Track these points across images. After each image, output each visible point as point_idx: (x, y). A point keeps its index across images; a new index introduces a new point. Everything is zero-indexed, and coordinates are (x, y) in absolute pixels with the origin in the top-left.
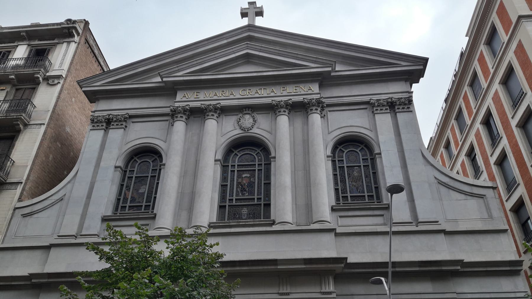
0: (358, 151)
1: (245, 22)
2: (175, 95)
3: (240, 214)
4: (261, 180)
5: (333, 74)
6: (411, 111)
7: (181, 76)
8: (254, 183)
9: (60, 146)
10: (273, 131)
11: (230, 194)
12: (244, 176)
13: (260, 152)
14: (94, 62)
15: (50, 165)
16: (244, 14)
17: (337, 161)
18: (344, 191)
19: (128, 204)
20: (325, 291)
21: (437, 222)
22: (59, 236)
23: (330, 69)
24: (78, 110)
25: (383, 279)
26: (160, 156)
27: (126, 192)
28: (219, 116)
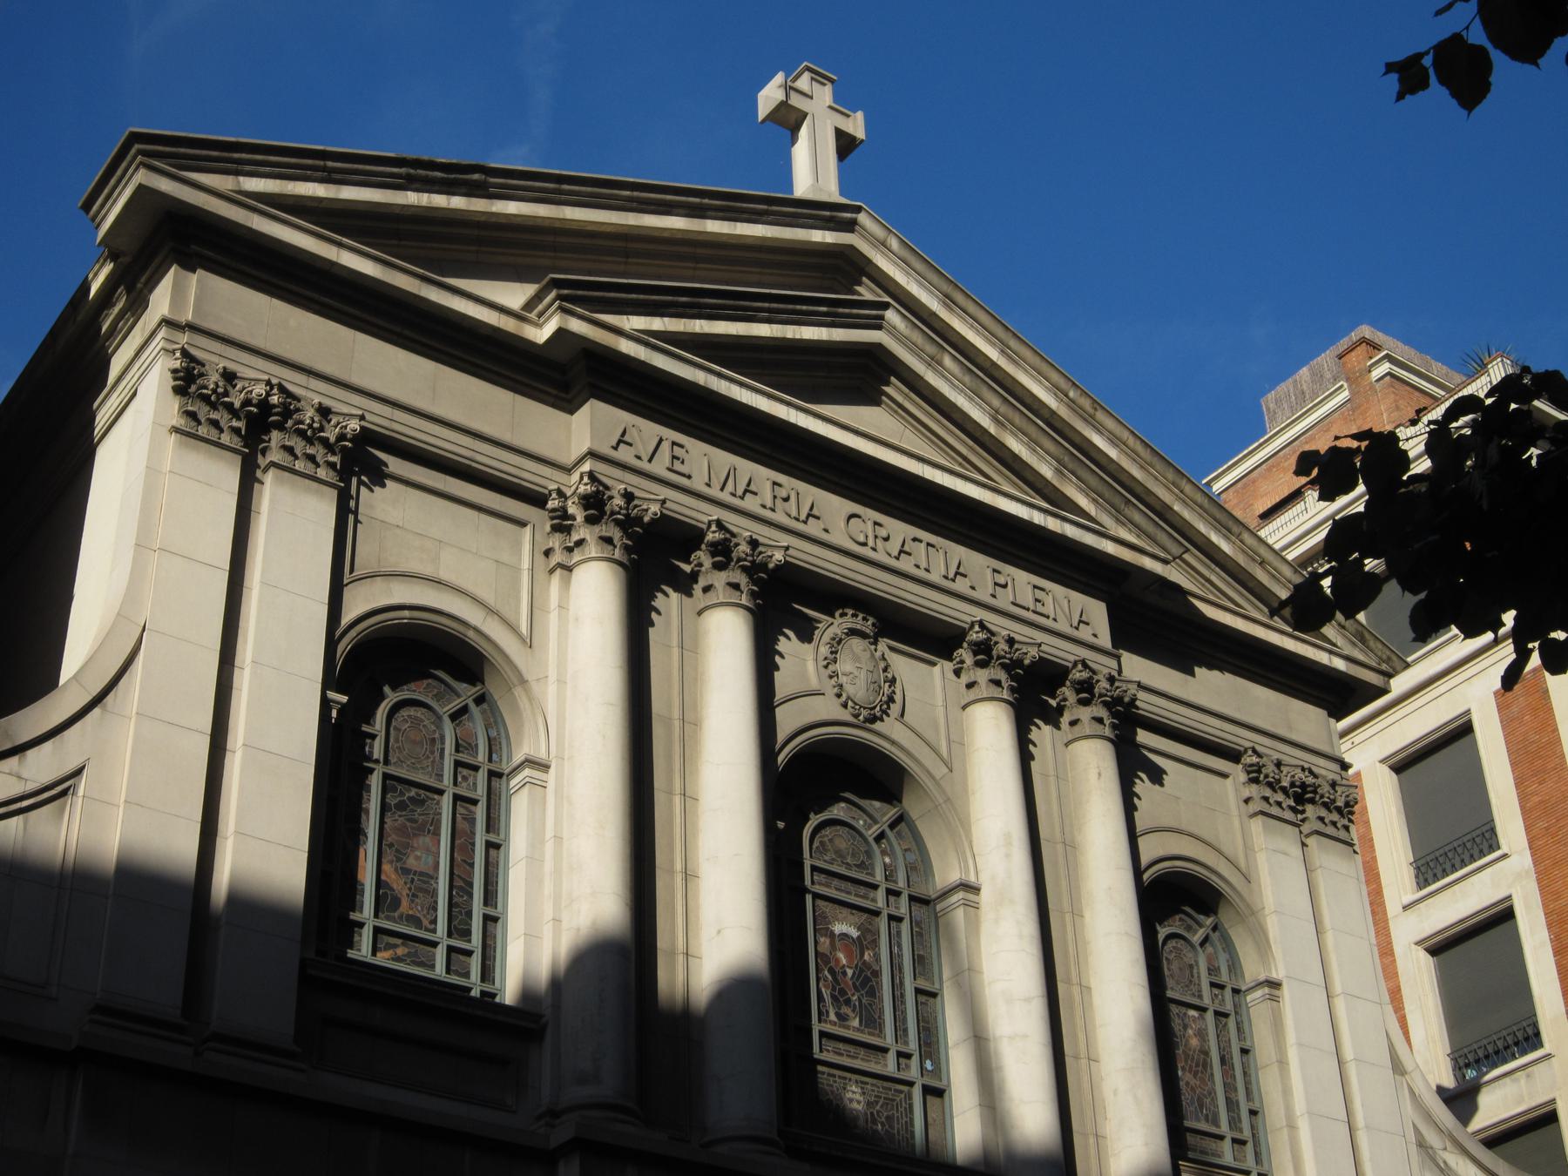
7: (631, 334)
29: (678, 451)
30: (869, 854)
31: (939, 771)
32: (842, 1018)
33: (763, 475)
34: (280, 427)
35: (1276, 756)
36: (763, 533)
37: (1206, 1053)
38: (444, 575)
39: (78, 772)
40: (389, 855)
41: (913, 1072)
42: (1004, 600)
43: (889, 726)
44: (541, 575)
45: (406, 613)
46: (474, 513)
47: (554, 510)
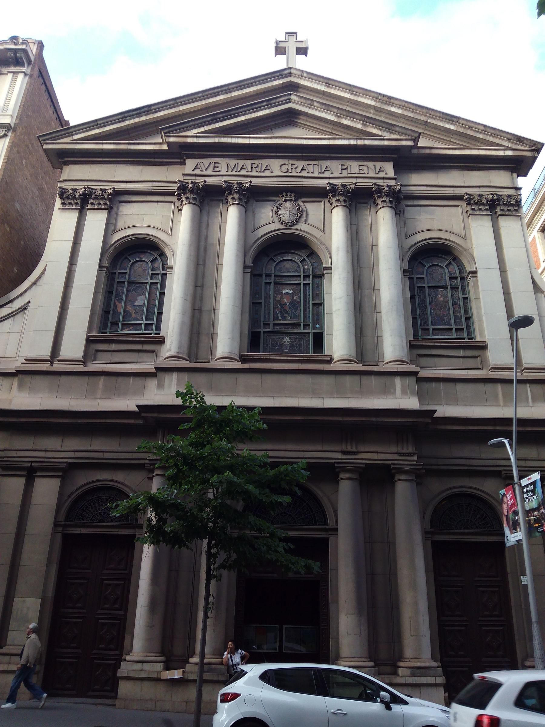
0: (444, 265)
1: (279, 63)
2: (183, 164)
4: (309, 299)
5: (415, 151)
6: (519, 216)
7: (192, 136)
8: (299, 302)
9: (8, 229)
10: (325, 229)
11: (265, 316)
12: (284, 292)
13: (306, 259)
14: (48, 106)
16: (280, 50)
17: (415, 278)
18: (424, 321)
19: (121, 321)
20: (408, 452)
22: (26, 360)
23: (411, 143)
24: (29, 178)
25: (505, 441)
26: (162, 255)
27: (117, 303)
28: (248, 201)
29: (216, 165)
30: (299, 267)
32: (284, 318)
33: (248, 163)
34: (499, 204)
37: (447, 302)
38: (145, 223)
39: (29, 302)
40: (129, 303)
41: (311, 330)
42: (345, 173)
43: (302, 226)
44: (466, 219)
45: (131, 237)
46: (155, 204)
47: (466, 199)
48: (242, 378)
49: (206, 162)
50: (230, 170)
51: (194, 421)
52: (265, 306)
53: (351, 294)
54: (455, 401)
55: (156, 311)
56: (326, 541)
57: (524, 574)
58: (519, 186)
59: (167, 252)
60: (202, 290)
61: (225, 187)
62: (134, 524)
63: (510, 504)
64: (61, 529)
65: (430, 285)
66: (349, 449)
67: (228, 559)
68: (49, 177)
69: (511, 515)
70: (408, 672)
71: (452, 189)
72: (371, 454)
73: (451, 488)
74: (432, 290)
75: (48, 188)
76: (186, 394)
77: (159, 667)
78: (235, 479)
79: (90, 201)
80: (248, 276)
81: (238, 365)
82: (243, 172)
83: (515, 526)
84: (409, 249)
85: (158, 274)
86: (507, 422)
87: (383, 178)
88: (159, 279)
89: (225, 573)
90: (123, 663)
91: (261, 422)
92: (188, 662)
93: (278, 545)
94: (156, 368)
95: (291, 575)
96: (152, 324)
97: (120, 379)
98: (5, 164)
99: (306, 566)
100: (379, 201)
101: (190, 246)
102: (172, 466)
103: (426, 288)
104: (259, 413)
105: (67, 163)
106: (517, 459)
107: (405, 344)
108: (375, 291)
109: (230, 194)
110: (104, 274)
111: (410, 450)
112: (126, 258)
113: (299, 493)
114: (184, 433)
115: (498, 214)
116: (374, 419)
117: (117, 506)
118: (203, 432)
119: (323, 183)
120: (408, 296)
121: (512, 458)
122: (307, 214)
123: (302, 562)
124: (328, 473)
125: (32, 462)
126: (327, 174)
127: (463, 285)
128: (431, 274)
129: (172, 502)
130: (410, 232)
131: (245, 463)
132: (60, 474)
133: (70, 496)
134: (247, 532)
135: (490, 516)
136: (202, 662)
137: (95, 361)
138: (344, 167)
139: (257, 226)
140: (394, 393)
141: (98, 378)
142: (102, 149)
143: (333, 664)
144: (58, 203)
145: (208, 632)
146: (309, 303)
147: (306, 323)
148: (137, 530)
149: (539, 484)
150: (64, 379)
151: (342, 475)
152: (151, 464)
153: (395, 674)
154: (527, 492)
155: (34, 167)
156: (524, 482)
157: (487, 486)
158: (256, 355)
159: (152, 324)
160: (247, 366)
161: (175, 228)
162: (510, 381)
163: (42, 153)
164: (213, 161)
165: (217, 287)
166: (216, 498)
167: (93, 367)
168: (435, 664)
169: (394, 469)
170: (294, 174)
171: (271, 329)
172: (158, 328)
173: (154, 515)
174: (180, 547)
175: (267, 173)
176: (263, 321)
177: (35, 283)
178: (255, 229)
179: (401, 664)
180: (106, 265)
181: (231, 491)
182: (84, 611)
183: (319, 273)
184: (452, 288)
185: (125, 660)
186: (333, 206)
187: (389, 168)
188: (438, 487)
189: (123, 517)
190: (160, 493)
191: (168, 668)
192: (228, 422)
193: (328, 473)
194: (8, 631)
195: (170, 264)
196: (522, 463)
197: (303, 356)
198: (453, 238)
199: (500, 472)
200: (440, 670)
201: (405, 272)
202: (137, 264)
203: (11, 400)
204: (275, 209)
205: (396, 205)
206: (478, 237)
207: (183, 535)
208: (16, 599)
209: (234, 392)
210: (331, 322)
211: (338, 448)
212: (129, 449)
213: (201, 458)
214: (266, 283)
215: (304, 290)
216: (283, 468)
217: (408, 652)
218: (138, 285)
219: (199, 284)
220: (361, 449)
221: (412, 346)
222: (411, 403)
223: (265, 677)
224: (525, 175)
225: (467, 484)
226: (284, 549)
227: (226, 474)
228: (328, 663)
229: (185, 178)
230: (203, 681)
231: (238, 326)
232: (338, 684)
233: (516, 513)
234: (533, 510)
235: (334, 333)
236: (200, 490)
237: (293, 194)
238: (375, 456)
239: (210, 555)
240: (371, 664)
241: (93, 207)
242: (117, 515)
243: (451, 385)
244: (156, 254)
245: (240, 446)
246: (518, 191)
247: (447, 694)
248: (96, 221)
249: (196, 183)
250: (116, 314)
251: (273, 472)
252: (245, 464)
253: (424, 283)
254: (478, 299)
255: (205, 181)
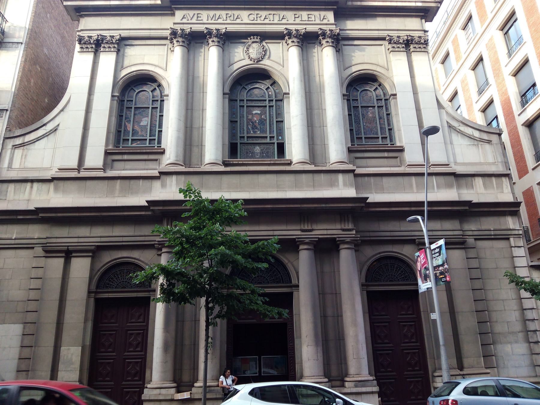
2: (173, 15)
3: (253, 153)
8: (266, 120)
9: (39, 69)
12: (254, 112)
13: (270, 87)
15: (32, 91)
18: (359, 132)
19: (130, 138)
20: (348, 228)
21: (448, 165)
22: (59, 169)
24: (54, 28)
25: (419, 217)
27: (127, 123)
28: (225, 43)
29: (199, 15)
30: (265, 93)
31: (279, 68)
32: (255, 132)
34: (412, 43)
35: (397, 35)
36: (218, 27)
37: (375, 117)
38: (145, 62)
39: (59, 125)
40: (136, 124)
41: (275, 141)
42: (298, 21)
46: (153, 46)
48: (225, 178)
49: (191, 13)
50: (210, 19)
51: (193, 211)
52: (240, 124)
53: (305, 113)
54: (382, 190)
55: (157, 129)
56: (291, 294)
57: (434, 311)
58: (426, 29)
59: (164, 83)
60: (192, 113)
61: (207, 33)
62: (149, 289)
63: (422, 263)
64: (93, 295)
65: (362, 105)
66: (306, 228)
67: (221, 311)
68: (69, 27)
69: (423, 271)
70: (352, 384)
71: (377, 32)
72: (323, 230)
73: (380, 253)
74: (364, 109)
75: (69, 36)
76: (187, 191)
77: (173, 391)
78: (227, 251)
79: (103, 45)
80: (227, 100)
81: (222, 168)
82: (220, 21)
83: (426, 278)
84: (347, 78)
85: (158, 101)
86: (421, 204)
87: (326, 24)
88: (158, 105)
89: (218, 320)
90: (145, 390)
91: (243, 211)
92: (193, 386)
93: (258, 299)
94: (161, 173)
95: (267, 320)
96: (155, 139)
97: (133, 182)
98: (33, 17)
99: (278, 313)
100: (324, 42)
101: (181, 78)
102: (178, 244)
103: (360, 107)
104: (242, 204)
105: (82, 16)
106: (428, 231)
107: (345, 150)
108: (322, 110)
109: (210, 38)
110: (115, 102)
111: (350, 226)
112: (132, 89)
113: (272, 260)
114: (185, 220)
115: (411, 51)
116: (324, 205)
117: (137, 276)
118: (200, 219)
119: (281, 28)
120: (347, 113)
121: (424, 230)
122: (270, 53)
123: (276, 310)
124: (291, 245)
125: (68, 246)
126: (284, 21)
127: (386, 105)
128: (363, 97)
129: (178, 271)
130: (347, 66)
131: (232, 241)
132: (91, 254)
133: (99, 271)
134: (235, 290)
135: (407, 272)
136: (205, 386)
137: (112, 168)
138: (297, 16)
139: (232, 62)
140: (338, 186)
141: (115, 181)
142: (110, 5)
143: (298, 381)
144: (78, 47)
145: (207, 362)
146: (273, 120)
147: (271, 135)
148: (151, 293)
149: (444, 248)
150: (89, 183)
151: (301, 247)
152: (159, 244)
153: (343, 386)
154: (435, 254)
155: (56, 20)
156: (433, 246)
157: (406, 251)
158: (235, 161)
159: (155, 139)
160: (228, 169)
161: (167, 64)
162: (423, 174)
163: (62, 8)
164: (196, 12)
165: (203, 110)
166: (211, 266)
167: (111, 173)
168: (371, 378)
169: (339, 241)
170: (259, 22)
171: (245, 141)
172: (159, 142)
173: (165, 281)
174: (185, 303)
175: (238, 21)
176: (239, 135)
177: (62, 110)
178: (231, 65)
179: (347, 379)
180: (117, 94)
181: (224, 261)
182: (114, 354)
183: (281, 98)
184: (378, 107)
185: (147, 388)
186: (289, 46)
187: (330, 16)
188: (371, 253)
189: (142, 284)
190: (169, 265)
191: (178, 392)
192: (218, 211)
193: (291, 245)
194: (58, 371)
195: (166, 93)
196: (431, 233)
197: (270, 161)
198: (378, 69)
199: (415, 240)
200: (375, 382)
201: (344, 95)
202: (141, 93)
203: (49, 200)
204: (245, 49)
205: (336, 45)
206: (395, 69)
207: (187, 295)
208: (62, 348)
209: (219, 188)
210: (291, 134)
211: (298, 227)
212: (142, 234)
213: (201, 238)
214: (240, 106)
215: (270, 111)
216: (261, 243)
217: (352, 370)
218: (142, 109)
219: (190, 107)
220: (315, 227)
221: (350, 151)
222: (350, 193)
223: (253, 393)
224: (431, 21)
225: (391, 250)
226: (262, 301)
227: (220, 248)
228: (294, 380)
229: (175, 26)
230: (206, 399)
231: (221, 139)
232: (303, 396)
233: (427, 269)
234: (439, 266)
235: (293, 143)
236: (199, 262)
237: (259, 37)
238: (325, 232)
239: (207, 308)
240: (326, 380)
241: (104, 50)
242: (137, 283)
243: (378, 179)
244: (155, 85)
245: (228, 228)
246: (426, 33)
247: (380, 399)
248: (107, 59)
249: (184, 30)
250: (126, 132)
251: (253, 247)
252: (233, 241)
253: (358, 103)
254: (397, 114)
255: (191, 28)
